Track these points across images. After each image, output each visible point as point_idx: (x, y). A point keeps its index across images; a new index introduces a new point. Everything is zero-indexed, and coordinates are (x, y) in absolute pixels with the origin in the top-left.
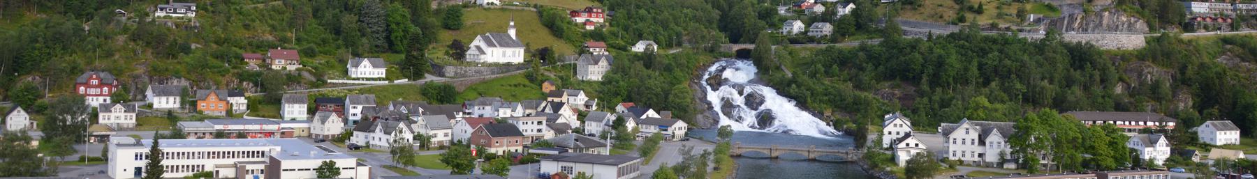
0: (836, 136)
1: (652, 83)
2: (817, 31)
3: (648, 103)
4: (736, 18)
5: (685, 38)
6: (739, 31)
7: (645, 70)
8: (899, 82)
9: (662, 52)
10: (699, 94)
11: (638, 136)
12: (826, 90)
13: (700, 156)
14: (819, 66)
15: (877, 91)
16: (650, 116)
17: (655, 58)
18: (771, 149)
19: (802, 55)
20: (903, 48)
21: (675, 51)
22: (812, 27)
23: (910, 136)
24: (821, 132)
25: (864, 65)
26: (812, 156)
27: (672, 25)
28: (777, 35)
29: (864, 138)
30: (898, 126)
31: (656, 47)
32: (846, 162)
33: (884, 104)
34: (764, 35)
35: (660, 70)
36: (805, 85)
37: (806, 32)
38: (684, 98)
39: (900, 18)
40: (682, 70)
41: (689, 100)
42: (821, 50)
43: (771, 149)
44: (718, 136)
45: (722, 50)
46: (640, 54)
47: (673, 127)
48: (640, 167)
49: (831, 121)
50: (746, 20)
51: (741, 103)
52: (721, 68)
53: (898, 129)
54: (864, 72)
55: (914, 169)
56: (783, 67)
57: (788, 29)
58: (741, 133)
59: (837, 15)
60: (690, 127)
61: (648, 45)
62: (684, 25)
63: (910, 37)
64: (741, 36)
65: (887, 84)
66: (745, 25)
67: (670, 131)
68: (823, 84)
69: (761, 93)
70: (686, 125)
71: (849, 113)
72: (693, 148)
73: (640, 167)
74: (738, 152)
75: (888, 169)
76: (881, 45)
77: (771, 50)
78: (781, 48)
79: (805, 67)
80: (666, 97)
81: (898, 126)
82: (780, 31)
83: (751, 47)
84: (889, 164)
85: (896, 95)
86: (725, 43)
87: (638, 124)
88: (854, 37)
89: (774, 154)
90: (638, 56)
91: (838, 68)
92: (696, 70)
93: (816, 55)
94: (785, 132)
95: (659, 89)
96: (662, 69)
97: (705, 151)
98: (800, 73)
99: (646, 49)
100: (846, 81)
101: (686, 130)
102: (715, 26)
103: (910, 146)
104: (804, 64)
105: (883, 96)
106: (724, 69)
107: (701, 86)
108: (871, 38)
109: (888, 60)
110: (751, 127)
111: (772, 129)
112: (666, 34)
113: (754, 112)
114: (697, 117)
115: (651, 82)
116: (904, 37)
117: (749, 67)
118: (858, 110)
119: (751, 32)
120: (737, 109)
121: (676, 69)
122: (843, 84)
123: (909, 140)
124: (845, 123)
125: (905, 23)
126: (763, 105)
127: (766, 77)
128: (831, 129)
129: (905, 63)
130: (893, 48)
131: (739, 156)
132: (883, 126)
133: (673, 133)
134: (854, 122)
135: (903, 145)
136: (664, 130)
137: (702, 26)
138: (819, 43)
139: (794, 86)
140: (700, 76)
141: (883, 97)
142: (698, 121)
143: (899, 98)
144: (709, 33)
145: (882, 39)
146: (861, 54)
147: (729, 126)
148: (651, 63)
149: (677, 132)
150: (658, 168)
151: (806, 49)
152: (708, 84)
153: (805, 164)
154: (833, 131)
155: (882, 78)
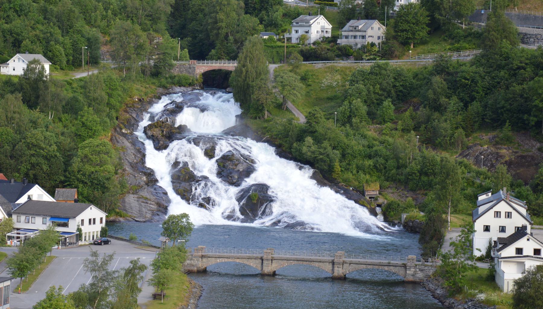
0: (387, 234)
1: (40, 136)
2: (355, 37)
3: (31, 173)
4: (202, 11)
5: (104, 49)
6: (208, 36)
7: (25, 109)
8: (510, 134)
9: (59, 76)
10: (131, 156)
11: (10, 238)
12: (369, 147)
13: (123, 273)
14: (358, 103)
15: (466, 151)
16: (35, 198)
17: (47, 88)
18: (262, 259)
19: (326, 82)
20: (519, 68)
21: (84, 75)
22: (346, 27)
23: (526, 234)
24: (359, 225)
25: (443, 100)
26: (339, 271)
27: (80, 24)
28: (279, 44)
29: (439, 238)
30: (503, 215)
31: (47, 66)
32: (403, 283)
33: (478, 174)
34: (254, 44)
35: (56, 110)
36: (329, 140)
37: (334, 39)
38: (101, 164)
39: (516, 11)
40: (97, 111)
41: (110, 168)
42: (362, 73)
43: (262, 259)
44: (163, 234)
45: (175, 72)
46: (16, 80)
47: (79, 218)
48: (12, 296)
49: (379, 206)
50: (221, 16)
51: (210, 171)
52: (170, 107)
53: (503, 221)
54: (442, 115)
55: (530, 297)
56: (290, 105)
57: (301, 31)
58: (208, 229)
59: (394, 5)
60: (112, 218)
61: (31, 63)
62: (103, 24)
63: (534, 47)
64: (212, 46)
65: (486, 136)
66: (220, 24)
67: (73, 226)
68: (364, 137)
69: (247, 153)
70: (103, 215)
71: (413, 190)
72: (111, 257)
73: (12, 296)
74: (201, 264)
75: (482, 296)
76: (476, 62)
77: (268, 72)
78: (286, 67)
79: (333, 104)
80: (67, 163)
81: (503, 215)
82: (287, 35)
83: (230, 66)
84: (483, 287)
85: (502, 157)
86: (181, 59)
87: (10, 215)
88: (425, 47)
89: (268, 268)
90: (13, 85)
91: (393, 107)
92: (126, 111)
93: (352, 82)
94: (290, 226)
95: (54, 147)
96: (60, 108)
97: (134, 262)
98: (321, 114)
99: (29, 70)
100: (408, 131)
101: (104, 225)
102: (162, 25)
103: (525, 253)
104: (330, 99)
105: (477, 158)
106: (178, 108)
107: (135, 142)
108: (458, 50)
109: (488, 90)
110: (229, 217)
111: (267, 221)
112: (67, 41)
113: (234, 191)
114: (127, 200)
115: (38, 134)
116: (522, 46)
117: (226, 105)
118: (430, 186)
119: (231, 38)
120: (203, 183)
121: (86, 108)
122: (402, 136)
123: (521, 243)
124: (405, 209)
125: (526, 20)
126: (253, 176)
127: (253, 124)
128: (378, 222)
129: (522, 96)
130: (500, 67)
131: (204, 272)
132: (475, 216)
133: (79, 230)
134: (422, 208)
135: (510, 251)
136: (59, 225)
137: (137, 27)
138: (359, 58)
139: (309, 140)
140: (133, 121)
141: (477, 161)
142: (128, 207)
143: (509, 164)
144: (151, 41)
145: (479, 51)
146: (437, 80)
147: (185, 216)
148: (38, 97)
149: (86, 229)
150: (43, 297)
151: (333, 70)
152: (149, 137)
153: (327, 287)
154: (382, 224)
155: (476, 125)
